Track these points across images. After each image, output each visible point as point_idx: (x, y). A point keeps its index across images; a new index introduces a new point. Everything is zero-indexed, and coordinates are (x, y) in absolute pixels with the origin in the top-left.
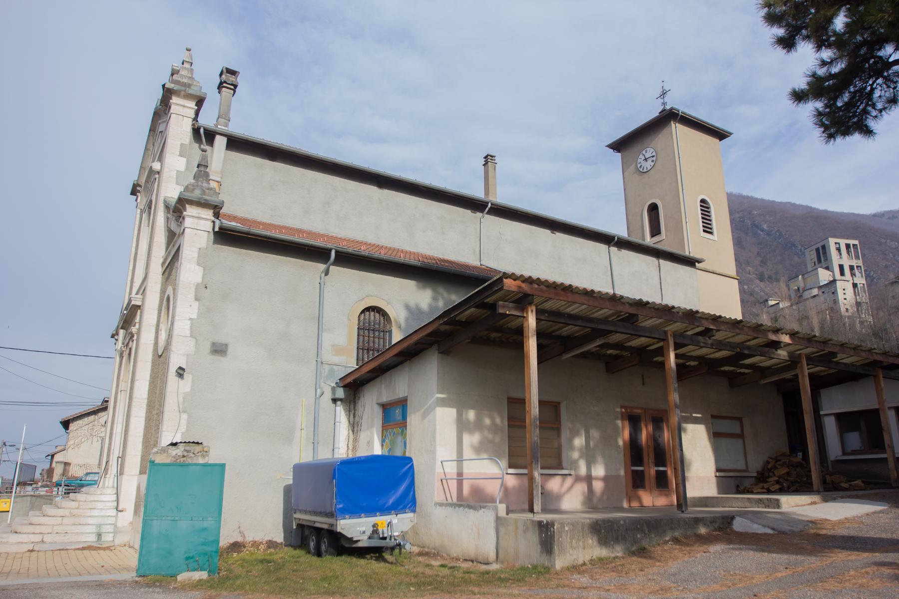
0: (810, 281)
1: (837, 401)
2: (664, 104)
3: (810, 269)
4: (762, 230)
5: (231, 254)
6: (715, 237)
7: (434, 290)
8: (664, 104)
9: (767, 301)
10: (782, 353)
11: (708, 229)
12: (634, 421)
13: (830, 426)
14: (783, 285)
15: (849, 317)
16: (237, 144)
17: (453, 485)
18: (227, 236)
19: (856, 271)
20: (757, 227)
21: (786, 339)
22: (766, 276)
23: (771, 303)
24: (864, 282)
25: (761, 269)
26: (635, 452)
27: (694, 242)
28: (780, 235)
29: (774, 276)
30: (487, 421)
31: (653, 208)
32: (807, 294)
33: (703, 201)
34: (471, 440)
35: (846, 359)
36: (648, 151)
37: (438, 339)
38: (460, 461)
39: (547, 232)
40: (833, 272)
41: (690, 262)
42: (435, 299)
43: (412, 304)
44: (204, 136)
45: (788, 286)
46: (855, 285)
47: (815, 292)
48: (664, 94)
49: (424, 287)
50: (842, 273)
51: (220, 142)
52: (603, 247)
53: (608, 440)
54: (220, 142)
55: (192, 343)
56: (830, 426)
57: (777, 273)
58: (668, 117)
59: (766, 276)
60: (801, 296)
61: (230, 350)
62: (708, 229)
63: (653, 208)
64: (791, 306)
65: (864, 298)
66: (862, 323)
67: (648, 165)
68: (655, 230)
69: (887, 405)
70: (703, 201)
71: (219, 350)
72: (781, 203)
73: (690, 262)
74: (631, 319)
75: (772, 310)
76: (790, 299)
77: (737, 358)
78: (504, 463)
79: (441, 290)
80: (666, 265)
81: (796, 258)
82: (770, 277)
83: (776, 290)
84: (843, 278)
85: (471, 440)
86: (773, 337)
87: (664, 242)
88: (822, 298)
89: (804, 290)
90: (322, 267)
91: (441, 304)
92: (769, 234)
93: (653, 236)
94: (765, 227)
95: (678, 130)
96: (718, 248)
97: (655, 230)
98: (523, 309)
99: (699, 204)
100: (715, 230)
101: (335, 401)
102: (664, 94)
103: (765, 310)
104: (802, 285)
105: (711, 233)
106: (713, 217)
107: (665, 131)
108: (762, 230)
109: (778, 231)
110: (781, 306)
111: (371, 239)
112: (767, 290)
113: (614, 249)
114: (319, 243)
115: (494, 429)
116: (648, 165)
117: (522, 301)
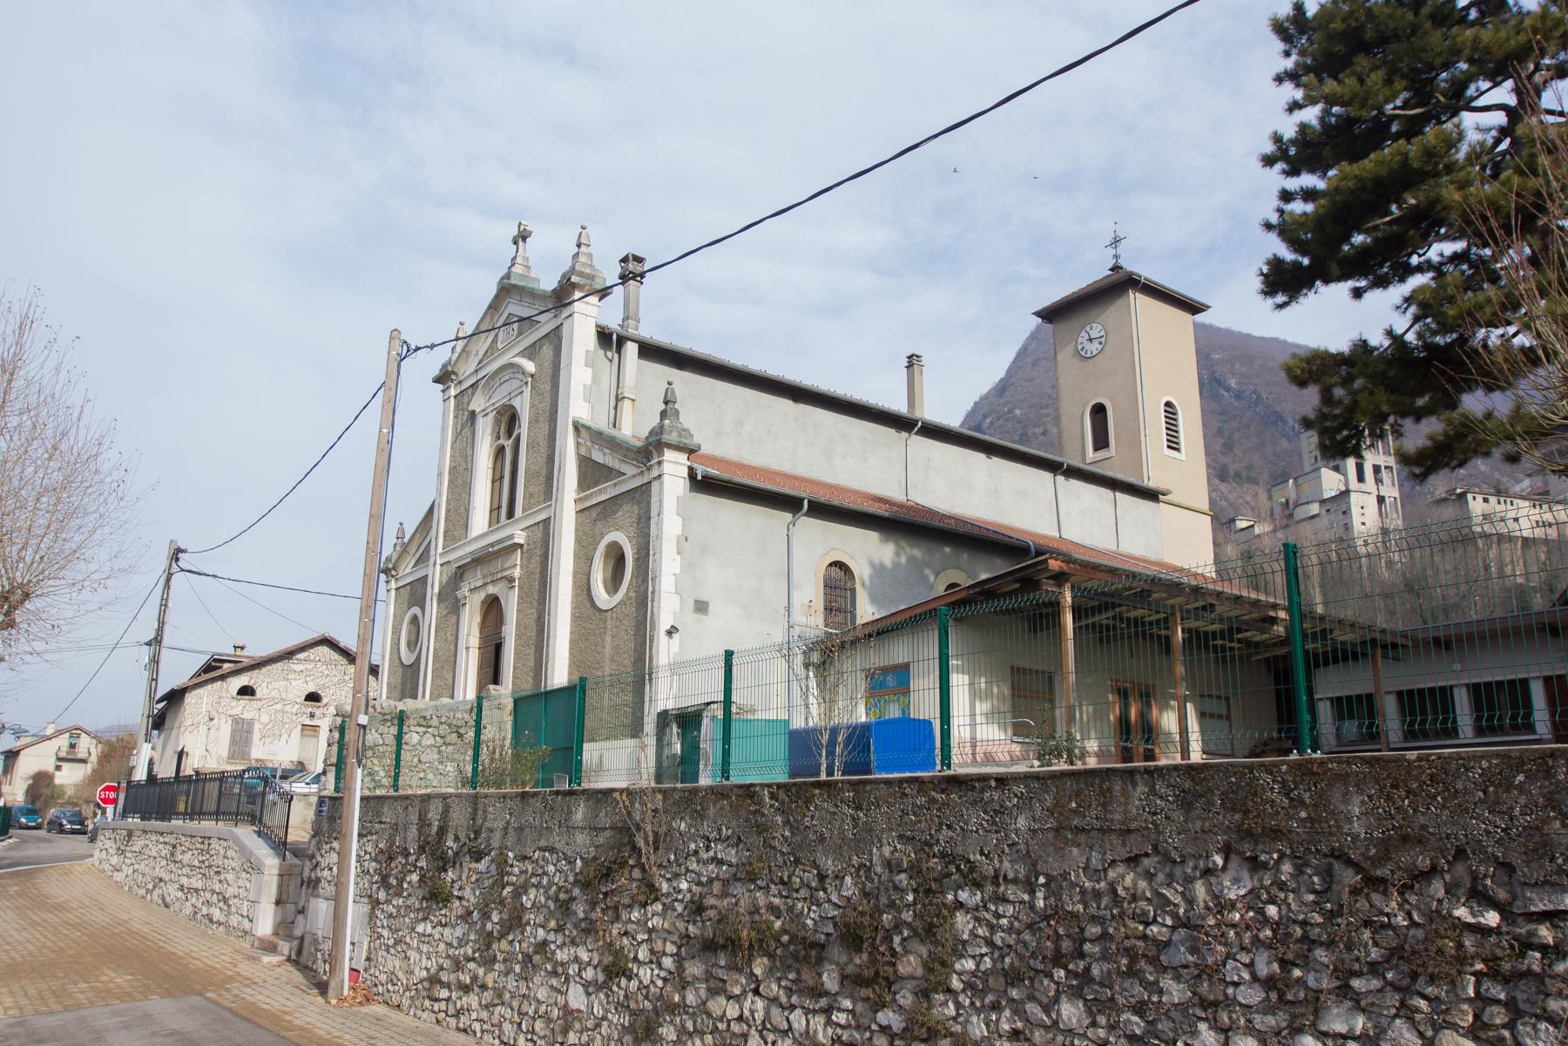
0: (1307, 490)
1: (1333, 684)
2: (1116, 257)
3: (1307, 468)
4: (1228, 389)
5: (705, 501)
6: (1182, 456)
7: (897, 544)
8: (1116, 257)
9: (1233, 520)
10: (1280, 629)
11: (1173, 445)
12: (1123, 694)
13: (1325, 711)
14: (1263, 496)
15: (1368, 556)
16: (652, 352)
17: (968, 750)
18: (704, 484)
19: (1385, 475)
20: (1219, 383)
21: (1282, 614)
22: (1232, 473)
23: (1241, 524)
24: (1397, 495)
25: (1224, 460)
26: (1124, 726)
27: (1157, 467)
28: (1259, 398)
29: (1244, 473)
30: (995, 690)
31: (1099, 411)
32: (1301, 513)
33: (1168, 404)
34: (982, 707)
35: (1341, 636)
36: (1095, 327)
37: (963, 607)
38: (973, 725)
39: (981, 456)
40: (1345, 475)
41: (1152, 495)
42: (897, 554)
43: (877, 561)
44: (607, 339)
45: (1270, 498)
46: (1381, 500)
47: (1315, 508)
48: (1116, 242)
49: (887, 540)
50: (1361, 478)
51: (631, 349)
52: (1047, 476)
53: (1099, 715)
54: (631, 349)
55: (677, 599)
56: (1325, 711)
57: (1250, 468)
58: (1120, 284)
59: (1232, 473)
60: (1291, 515)
61: (711, 608)
62: (1173, 445)
63: (1099, 411)
64: (1274, 531)
65: (1396, 521)
66: (1390, 563)
67: (1094, 348)
68: (1101, 442)
69: (1385, 687)
70: (1168, 404)
71: (701, 607)
72: (1262, 339)
73: (1152, 495)
74: (1143, 595)
75: (1243, 536)
76: (1274, 520)
77: (1228, 634)
78: (1010, 732)
79: (903, 543)
80: (1124, 499)
81: (1285, 443)
82: (1238, 474)
83: (1248, 498)
84: (1362, 487)
85: (982, 707)
86: (1272, 614)
87: (1112, 462)
88: (1324, 522)
89: (1297, 505)
90: (788, 516)
91: (903, 560)
92: (1238, 396)
93: (1096, 449)
94: (1233, 383)
95: (1139, 303)
96: (1183, 470)
97: (1101, 442)
98: (1060, 586)
99: (1162, 408)
100: (1183, 446)
101: (807, 666)
102: (1116, 242)
103: (1233, 537)
104: (1293, 495)
105: (1177, 450)
106: (1181, 428)
107: (1120, 302)
108: (1228, 389)
109: (1255, 392)
110: (1257, 530)
111: (787, 467)
112: (1233, 497)
113: (1060, 479)
114: (787, 490)
115: (1001, 698)
116: (1094, 348)
117: (1060, 578)
